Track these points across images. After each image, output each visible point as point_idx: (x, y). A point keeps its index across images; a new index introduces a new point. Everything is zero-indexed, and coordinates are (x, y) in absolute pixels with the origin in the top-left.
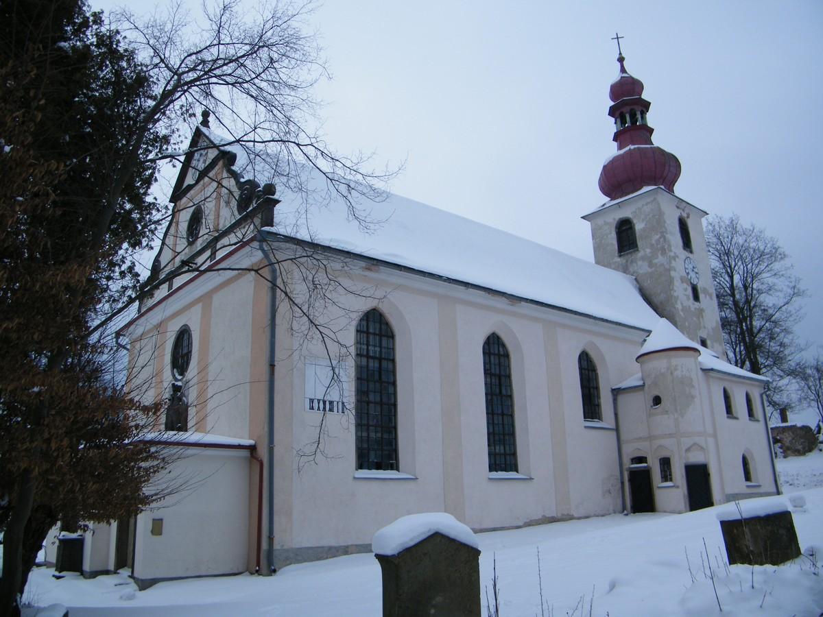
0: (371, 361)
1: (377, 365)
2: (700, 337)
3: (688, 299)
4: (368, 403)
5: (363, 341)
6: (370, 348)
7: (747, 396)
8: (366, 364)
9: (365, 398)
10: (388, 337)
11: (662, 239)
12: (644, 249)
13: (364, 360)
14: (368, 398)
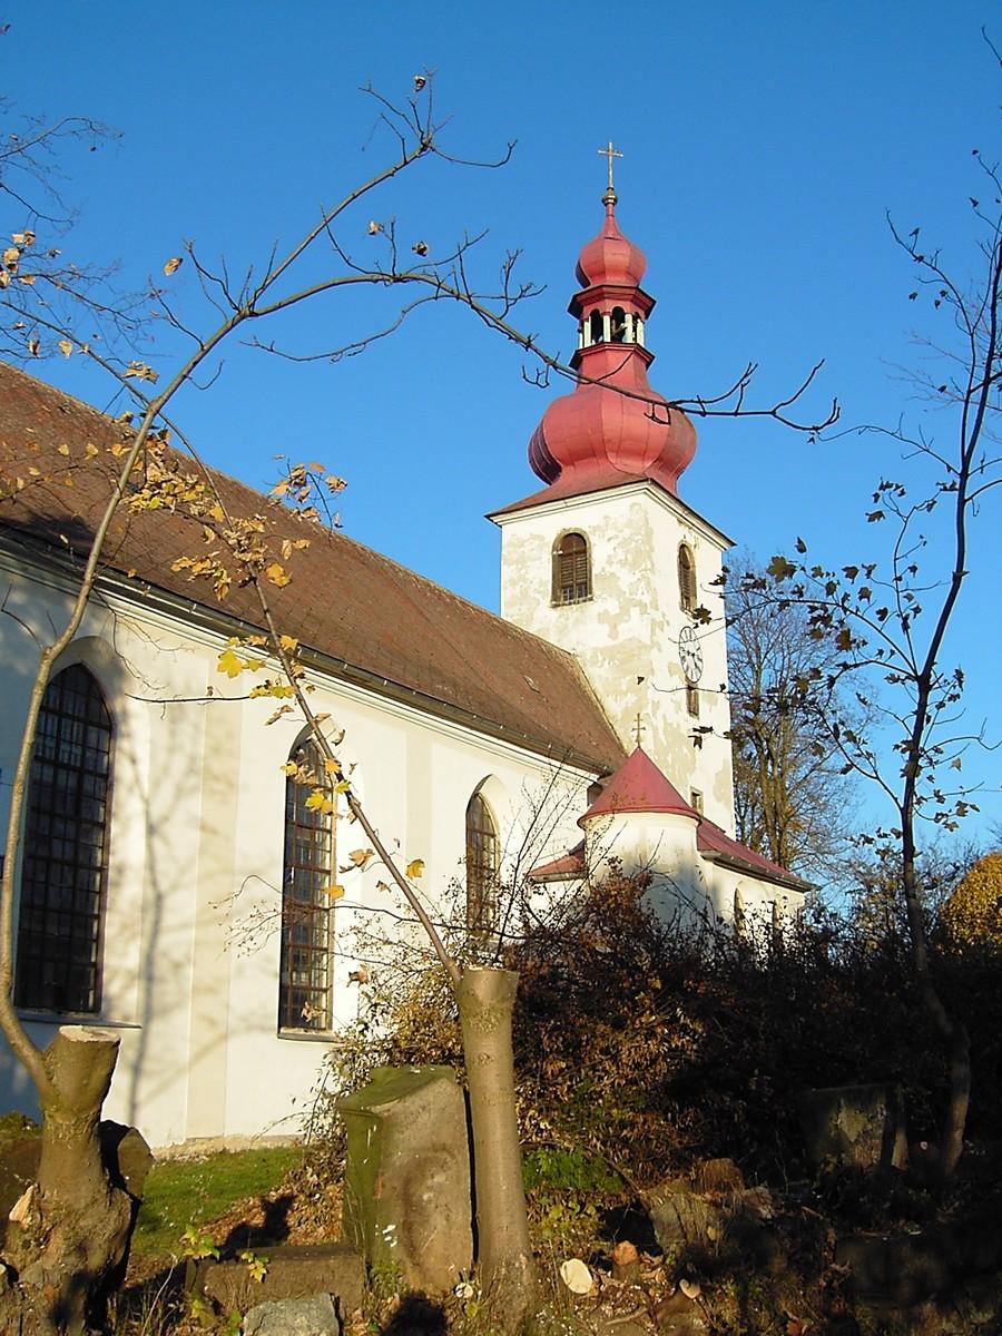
0: (62, 775)
1: (72, 781)
2: (691, 788)
3: (679, 708)
4: (49, 861)
5: (52, 731)
6: (88, 754)
7: (476, 809)
8: (50, 780)
9: (43, 852)
10: (99, 726)
11: (642, 584)
12: (603, 600)
13: (48, 773)
14: (50, 849)
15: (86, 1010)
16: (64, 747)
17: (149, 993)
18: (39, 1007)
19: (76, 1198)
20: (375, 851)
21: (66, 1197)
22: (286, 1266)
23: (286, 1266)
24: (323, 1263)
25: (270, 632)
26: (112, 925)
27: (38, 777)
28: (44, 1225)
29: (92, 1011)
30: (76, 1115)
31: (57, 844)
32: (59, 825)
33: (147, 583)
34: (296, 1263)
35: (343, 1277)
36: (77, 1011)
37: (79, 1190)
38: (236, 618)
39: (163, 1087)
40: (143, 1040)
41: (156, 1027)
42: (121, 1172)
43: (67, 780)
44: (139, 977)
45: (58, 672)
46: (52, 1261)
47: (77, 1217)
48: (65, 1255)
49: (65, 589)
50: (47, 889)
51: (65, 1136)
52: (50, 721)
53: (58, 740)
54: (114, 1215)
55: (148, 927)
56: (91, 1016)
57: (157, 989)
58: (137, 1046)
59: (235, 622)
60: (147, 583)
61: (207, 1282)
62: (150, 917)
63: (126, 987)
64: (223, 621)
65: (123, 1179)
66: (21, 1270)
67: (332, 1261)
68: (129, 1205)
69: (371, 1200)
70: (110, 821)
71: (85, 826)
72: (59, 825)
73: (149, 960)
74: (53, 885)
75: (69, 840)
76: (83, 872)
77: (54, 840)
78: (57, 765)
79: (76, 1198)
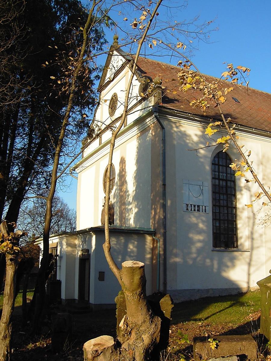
0: (221, 182)
1: (224, 184)
4: (219, 206)
5: (221, 171)
8: (218, 184)
13: (217, 181)
15: (234, 247)
16: (221, 174)
17: (252, 242)
18: (220, 247)
19: (138, 321)
20: (263, 192)
21: (134, 320)
22: (225, 344)
23: (225, 344)
24: (240, 343)
25: (223, 121)
26: (240, 224)
27: (214, 183)
28: (128, 329)
29: (236, 248)
30: (131, 292)
31: (221, 202)
32: (222, 197)
33: (239, 125)
34: (230, 343)
35: (248, 348)
36: (231, 248)
37: (138, 317)
38: (267, 131)
39: (258, 269)
40: (251, 255)
41: (255, 252)
42: (162, 310)
43: (223, 183)
44: (248, 238)
45: (216, 153)
46: (132, 341)
47: (139, 327)
48: (136, 340)
49: (223, 132)
50: (220, 215)
51: (130, 299)
52: (224, 168)
53: (219, 172)
54: (153, 326)
55: (251, 224)
56: (235, 249)
57: (255, 242)
58: (249, 257)
59: (266, 132)
60: (239, 125)
61: (196, 349)
62: (252, 221)
63: (245, 241)
64: (262, 132)
65: (163, 312)
66: (123, 344)
67: (244, 343)
68: (160, 322)
69: (269, 317)
70: (236, 194)
71: (229, 196)
72: (222, 197)
73: (252, 233)
74: (221, 213)
75: (222, 200)
76: (230, 209)
77: (221, 200)
78: (219, 179)
79: (138, 321)
